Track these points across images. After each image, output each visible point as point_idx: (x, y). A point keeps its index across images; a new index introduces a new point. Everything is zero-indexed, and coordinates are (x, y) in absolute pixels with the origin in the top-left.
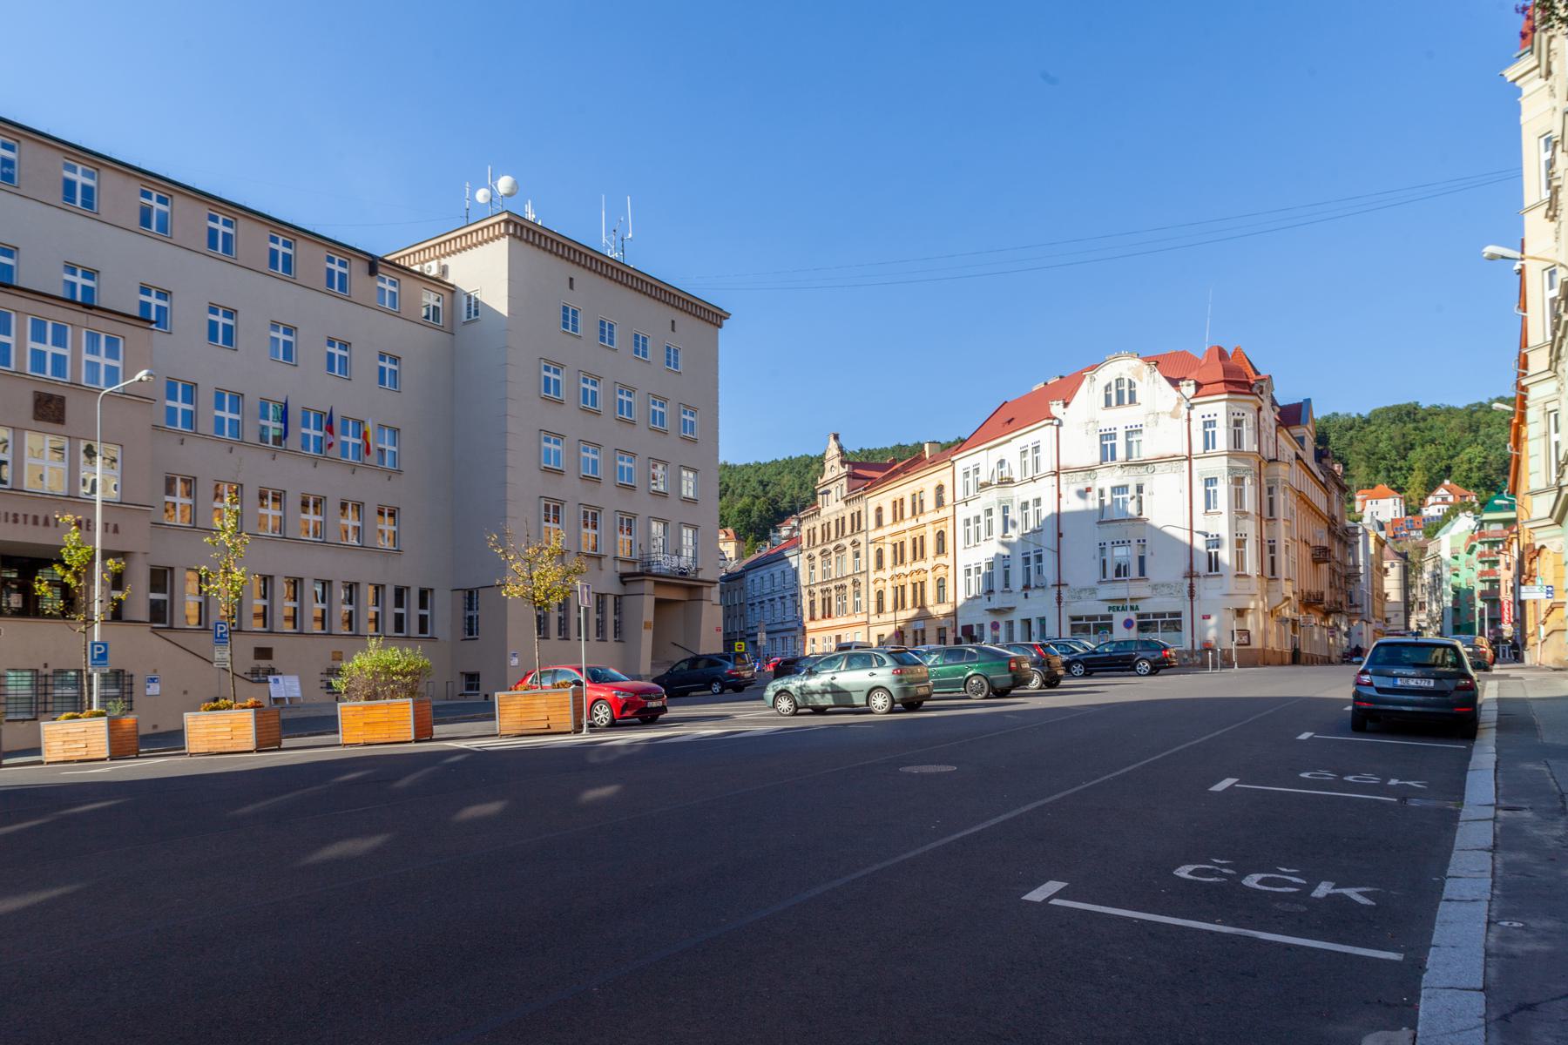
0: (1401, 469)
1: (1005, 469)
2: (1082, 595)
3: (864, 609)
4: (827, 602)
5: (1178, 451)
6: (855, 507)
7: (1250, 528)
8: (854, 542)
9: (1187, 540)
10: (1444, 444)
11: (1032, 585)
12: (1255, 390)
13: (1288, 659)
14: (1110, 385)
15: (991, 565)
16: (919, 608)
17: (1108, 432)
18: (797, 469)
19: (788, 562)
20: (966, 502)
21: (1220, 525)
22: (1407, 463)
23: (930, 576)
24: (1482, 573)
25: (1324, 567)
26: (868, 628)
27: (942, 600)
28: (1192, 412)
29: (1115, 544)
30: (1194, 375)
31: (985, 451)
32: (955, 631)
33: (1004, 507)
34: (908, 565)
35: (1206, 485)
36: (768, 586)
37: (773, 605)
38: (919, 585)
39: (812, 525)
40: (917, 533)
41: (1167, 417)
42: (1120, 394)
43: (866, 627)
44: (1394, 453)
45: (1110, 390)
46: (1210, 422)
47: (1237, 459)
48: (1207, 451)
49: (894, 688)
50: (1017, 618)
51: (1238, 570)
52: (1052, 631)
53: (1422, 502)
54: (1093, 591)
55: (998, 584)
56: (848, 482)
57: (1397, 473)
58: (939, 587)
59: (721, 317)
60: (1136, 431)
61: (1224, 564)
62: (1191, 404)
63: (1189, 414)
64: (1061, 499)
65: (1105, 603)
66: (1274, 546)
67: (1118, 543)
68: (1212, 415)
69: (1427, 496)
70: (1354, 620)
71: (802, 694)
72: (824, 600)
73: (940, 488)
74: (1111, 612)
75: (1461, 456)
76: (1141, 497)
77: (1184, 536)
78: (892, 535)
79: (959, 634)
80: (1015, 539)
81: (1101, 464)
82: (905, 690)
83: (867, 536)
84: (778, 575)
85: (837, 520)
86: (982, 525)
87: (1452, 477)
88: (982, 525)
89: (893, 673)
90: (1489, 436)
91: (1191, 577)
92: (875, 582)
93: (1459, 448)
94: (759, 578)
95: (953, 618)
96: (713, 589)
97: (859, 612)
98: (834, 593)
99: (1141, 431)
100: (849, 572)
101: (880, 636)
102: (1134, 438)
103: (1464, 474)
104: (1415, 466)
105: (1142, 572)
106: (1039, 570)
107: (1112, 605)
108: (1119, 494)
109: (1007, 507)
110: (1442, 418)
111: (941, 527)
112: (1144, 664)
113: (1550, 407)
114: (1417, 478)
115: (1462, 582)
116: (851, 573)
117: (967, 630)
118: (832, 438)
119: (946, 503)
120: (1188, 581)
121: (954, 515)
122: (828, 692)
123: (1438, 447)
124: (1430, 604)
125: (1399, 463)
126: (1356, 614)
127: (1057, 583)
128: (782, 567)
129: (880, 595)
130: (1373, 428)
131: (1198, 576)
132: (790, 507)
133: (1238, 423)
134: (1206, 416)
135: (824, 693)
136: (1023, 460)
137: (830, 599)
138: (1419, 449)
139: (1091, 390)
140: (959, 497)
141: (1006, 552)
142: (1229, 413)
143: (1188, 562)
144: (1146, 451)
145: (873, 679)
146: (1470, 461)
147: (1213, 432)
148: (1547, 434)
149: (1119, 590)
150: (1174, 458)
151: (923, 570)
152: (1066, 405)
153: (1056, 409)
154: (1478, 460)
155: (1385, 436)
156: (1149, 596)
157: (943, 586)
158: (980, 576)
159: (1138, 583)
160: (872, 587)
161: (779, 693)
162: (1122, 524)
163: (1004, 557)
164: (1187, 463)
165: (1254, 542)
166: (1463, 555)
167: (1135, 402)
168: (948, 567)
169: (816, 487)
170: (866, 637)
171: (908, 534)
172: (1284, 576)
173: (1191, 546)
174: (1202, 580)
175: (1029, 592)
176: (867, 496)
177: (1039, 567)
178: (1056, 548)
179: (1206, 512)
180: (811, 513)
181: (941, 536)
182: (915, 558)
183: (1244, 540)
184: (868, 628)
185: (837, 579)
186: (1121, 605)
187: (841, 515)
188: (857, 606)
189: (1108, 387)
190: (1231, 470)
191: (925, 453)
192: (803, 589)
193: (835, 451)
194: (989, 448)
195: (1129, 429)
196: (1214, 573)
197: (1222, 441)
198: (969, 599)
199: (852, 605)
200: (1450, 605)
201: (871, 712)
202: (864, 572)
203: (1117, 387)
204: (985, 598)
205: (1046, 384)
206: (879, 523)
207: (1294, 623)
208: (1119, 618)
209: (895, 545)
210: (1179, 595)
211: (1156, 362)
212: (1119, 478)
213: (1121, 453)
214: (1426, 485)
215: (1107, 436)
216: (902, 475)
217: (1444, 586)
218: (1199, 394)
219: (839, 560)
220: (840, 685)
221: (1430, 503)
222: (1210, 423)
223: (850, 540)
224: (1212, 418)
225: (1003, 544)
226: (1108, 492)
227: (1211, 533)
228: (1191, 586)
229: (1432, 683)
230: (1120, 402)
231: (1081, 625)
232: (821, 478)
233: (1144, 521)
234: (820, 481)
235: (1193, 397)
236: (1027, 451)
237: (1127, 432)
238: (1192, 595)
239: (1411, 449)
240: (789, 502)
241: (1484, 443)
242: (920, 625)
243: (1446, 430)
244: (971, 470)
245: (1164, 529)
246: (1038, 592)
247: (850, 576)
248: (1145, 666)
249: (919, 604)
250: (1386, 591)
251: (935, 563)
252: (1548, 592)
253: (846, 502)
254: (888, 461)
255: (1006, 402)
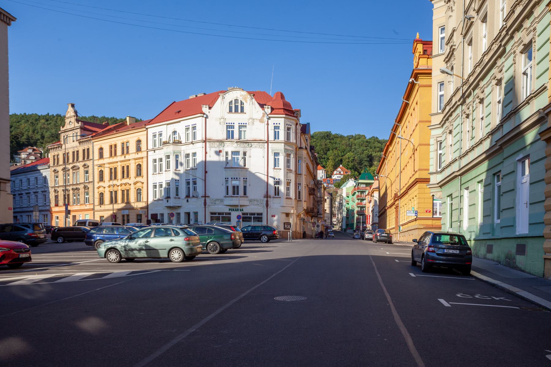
0: (324, 158)
1: (177, 136)
2: (217, 202)
3: (91, 202)
4: (66, 197)
5: (262, 138)
6: (85, 146)
7: (292, 177)
8: (85, 165)
9: (266, 180)
10: (340, 150)
11: (191, 195)
12: (295, 115)
13: (302, 236)
14: (232, 101)
15: (168, 184)
16: (126, 203)
17: (230, 124)
18: (30, 121)
19: (40, 173)
20: (154, 150)
21: (280, 175)
22: (327, 156)
23: (132, 187)
24: (358, 204)
25: (312, 196)
26: (94, 212)
27: (139, 200)
28: (269, 121)
29: (233, 179)
30: (270, 103)
31: (166, 125)
32: (147, 216)
33: (176, 155)
34: (119, 180)
35: (275, 156)
36: (26, 185)
37: (37, 196)
38: (125, 192)
39: (56, 153)
40: (125, 164)
41: (258, 122)
42: (236, 107)
43: (92, 212)
44: (322, 151)
45: (232, 104)
46: (277, 126)
47: (288, 145)
48: (275, 140)
49: (185, 248)
50: (182, 211)
51: (287, 196)
52: (201, 218)
53: (332, 174)
54: (222, 201)
55: (173, 194)
56: (81, 132)
57: (323, 160)
58: (137, 193)
59: (10, 19)
60: (244, 126)
61: (282, 192)
62: (269, 117)
63: (268, 121)
64: (207, 154)
65: (227, 207)
66: (178, 188)
67: (234, 178)
68: (278, 124)
69: (334, 171)
70: (319, 220)
71: (125, 250)
72: (64, 196)
73: (139, 142)
74: (230, 211)
75: (346, 156)
76: (245, 158)
77: (264, 178)
78: (109, 163)
79: (150, 218)
80: (182, 172)
81: (227, 140)
82: (191, 249)
83: (93, 163)
84: (32, 179)
85: (74, 152)
86: (164, 163)
87: (343, 164)
88: (164, 163)
89: (185, 240)
90: (355, 149)
91: (267, 197)
92: (99, 188)
93: (345, 152)
94: (19, 180)
95: (146, 210)
96: (7, 184)
97: (88, 203)
98: (71, 192)
99: (246, 126)
100: (82, 181)
101: (101, 217)
102: (243, 129)
103: (347, 163)
104: (330, 158)
105: (245, 193)
106: (195, 189)
107: (231, 208)
108: (235, 155)
109: (178, 155)
110: (339, 139)
111: (139, 162)
112: (265, 237)
113: (439, 139)
114: (330, 163)
115: (350, 206)
116: (83, 181)
117: (154, 216)
118: (70, 106)
119: (143, 150)
120: (266, 199)
121: (147, 157)
122: (143, 250)
123: (338, 151)
124: (338, 215)
125: (324, 156)
126: (320, 218)
127: (204, 195)
128: (36, 175)
129: (102, 195)
130: (315, 140)
131: (270, 197)
132: (27, 142)
133: (289, 129)
134: (275, 124)
135: (140, 250)
136: (187, 132)
137: (68, 195)
138: (331, 151)
139: (223, 103)
140: (150, 146)
141: (177, 178)
142: (286, 124)
143: (266, 190)
144: (249, 135)
145: (172, 243)
146: (349, 158)
147: (278, 132)
148: (437, 150)
149: (235, 201)
150: (260, 141)
151: (128, 184)
152: (210, 108)
153: (205, 109)
154: (351, 158)
155: (319, 144)
156: (248, 205)
157: (140, 193)
158: (163, 189)
159: (243, 198)
160: (96, 191)
161: (109, 250)
162: (236, 169)
163: (176, 180)
164: (266, 144)
165: (294, 184)
166: (351, 196)
167: (243, 112)
168: (143, 183)
169: (59, 132)
170: (93, 217)
171: (119, 164)
172: (304, 200)
173: (267, 183)
174: (272, 199)
175: (189, 199)
176: (93, 141)
177: (194, 187)
178: (204, 179)
179: (274, 168)
180: (56, 146)
181: (139, 167)
182: (123, 177)
183: (290, 183)
184: (94, 212)
185: (73, 185)
186: (235, 209)
187: (76, 149)
188: (87, 200)
189: (231, 103)
190: (286, 150)
191: (126, 122)
192: (50, 189)
193: (73, 114)
194: (168, 124)
195: (240, 125)
196: (277, 196)
197: (282, 137)
198: (155, 200)
199: (83, 199)
200: (345, 216)
201: (170, 261)
202: (91, 182)
203: (235, 103)
204: (165, 201)
205: (196, 96)
206: (101, 156)
207: (304, 219)
208: (234, 215)
209: (111, 169)
210: (262, 205)
211: (254, 94)
212: (235, 147)
213: (236, 136)
214: (334, 166)
215: (230, 127)
216: (115, 132)
217: (343, 208)
218: (272, 113)
219: (75, 174)
220: (151, 245)
221: (335, 174)
222: (277, 127)
223: (82, 164)
224: (278, 125)
225: (176, 174)
226: (230, 153)
227: (276, 178)
228: (267, 201)
229: (458, 252)
230: (236, 111)
231: (216, 217)
232: (63, 127)
233: (247, 169)
234: (62, 129)
235: (270, 114)
236: (189, 128)
237: (239, 126)
238: (267, 205)
239: (328, 151)
240: (26, 139)
241: (353, 151)
242: (126, 212)
243: (341, 145)
244: (157, 134)
245: (256, 174)
246: (194, 200)
247: (82, 183)
248: (265, 238)
249: (126, 201)
250: (325, 209)
251: (135, 181)
252: (416, 213)
253: (80, 143)
254: (104, 123)
255: (175, 102)
